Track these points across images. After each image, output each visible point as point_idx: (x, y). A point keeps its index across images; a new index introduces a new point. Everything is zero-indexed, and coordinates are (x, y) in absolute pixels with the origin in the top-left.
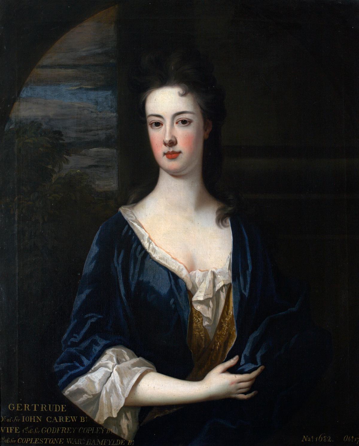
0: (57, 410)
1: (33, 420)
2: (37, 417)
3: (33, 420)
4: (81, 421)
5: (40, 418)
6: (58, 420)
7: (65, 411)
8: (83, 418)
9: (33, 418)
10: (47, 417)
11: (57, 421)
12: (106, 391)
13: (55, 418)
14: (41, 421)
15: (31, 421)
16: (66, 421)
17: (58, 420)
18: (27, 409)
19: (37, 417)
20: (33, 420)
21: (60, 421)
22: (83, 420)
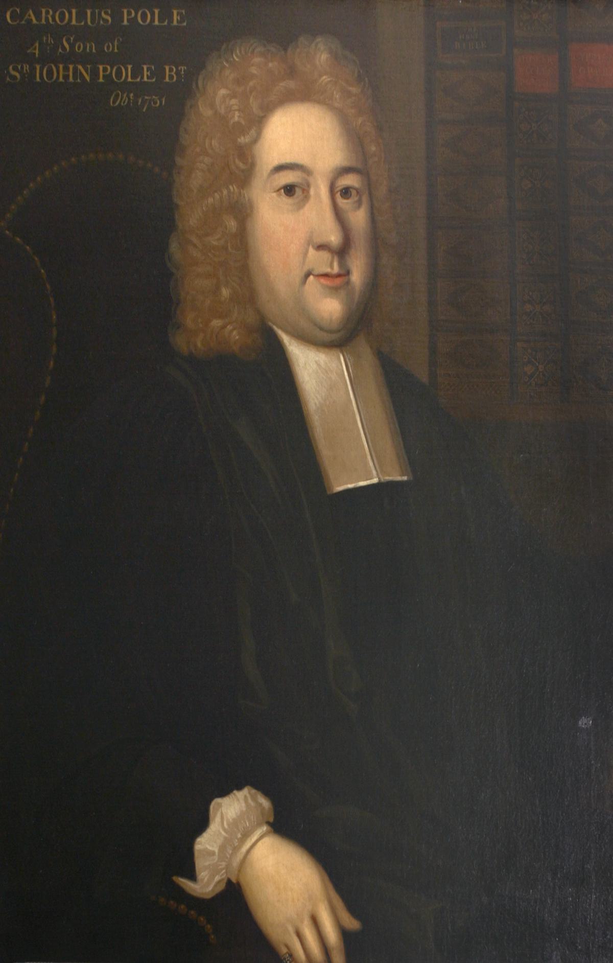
0: (159, 21)
1: (68, 76)
2: (80, 67)
3: (66, 77)
4: (167, 80)
5: (86, 71)
6: (38, 17)
7: (185, 24)
8: (171, 70)
9: (66, 69)
10: (6, 12)
11: (34, 21)
12: (195, 246)
13: (31, 12)
14: (88, 78)
15: (61, 79)
16: (145, 79)
17: (38, 17)
18: (47, 19)
19: (80, 67)
20: (66, 77)
21: (43, 22)
22: (171, 77)
